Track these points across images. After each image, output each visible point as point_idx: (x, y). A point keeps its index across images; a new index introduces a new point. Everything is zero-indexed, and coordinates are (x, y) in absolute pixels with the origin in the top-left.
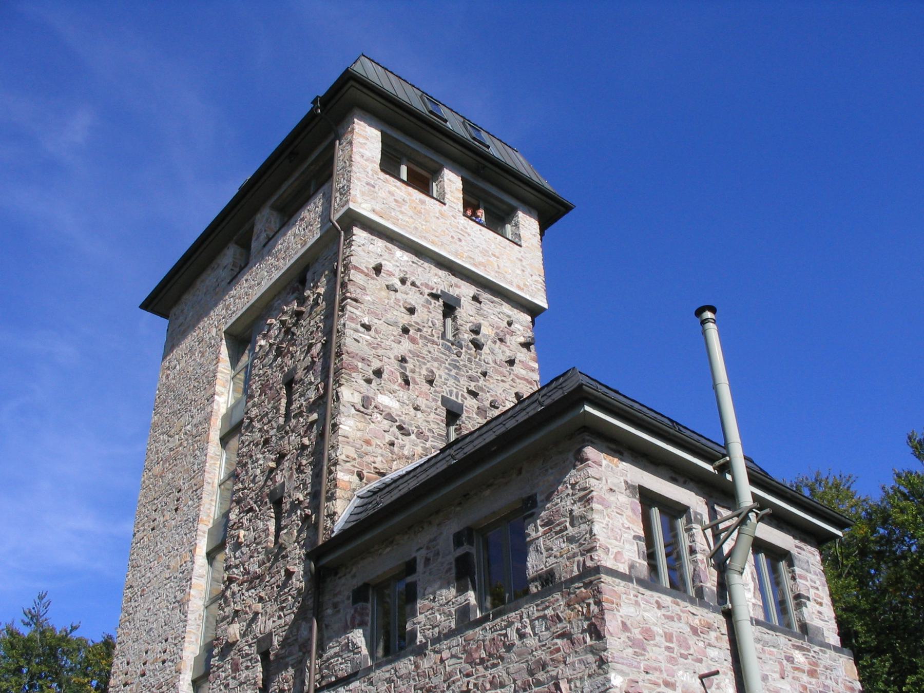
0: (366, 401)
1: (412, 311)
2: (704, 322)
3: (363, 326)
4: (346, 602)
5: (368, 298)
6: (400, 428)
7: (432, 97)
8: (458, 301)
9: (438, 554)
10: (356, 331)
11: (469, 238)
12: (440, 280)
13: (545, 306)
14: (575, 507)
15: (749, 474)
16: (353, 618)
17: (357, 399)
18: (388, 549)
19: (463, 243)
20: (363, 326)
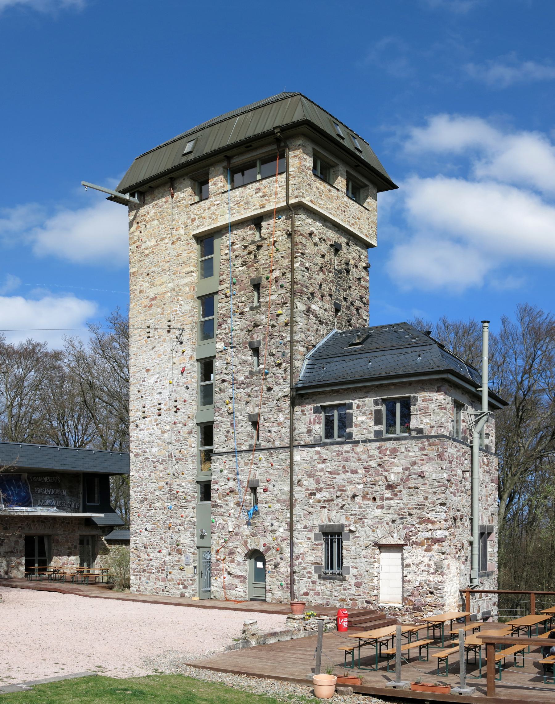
0: (309, 310)
1: (323, 256)
2: (483, 327)
3: (306, 268)
4: (310, 412)
5: (307, 251)
6: (320, 321)
7: (336, 119)
8: (340, 245)
9: (365, 405)
10: (303, 271)
11: (348, 209)
12: (332, 236)
13: (375, 244)
14: (436, 408)
15: (489, 392)
16: (314, 420)
17: (304, 308)
18: (335, 394)
19: (346, 213)
20: (306, 268)
